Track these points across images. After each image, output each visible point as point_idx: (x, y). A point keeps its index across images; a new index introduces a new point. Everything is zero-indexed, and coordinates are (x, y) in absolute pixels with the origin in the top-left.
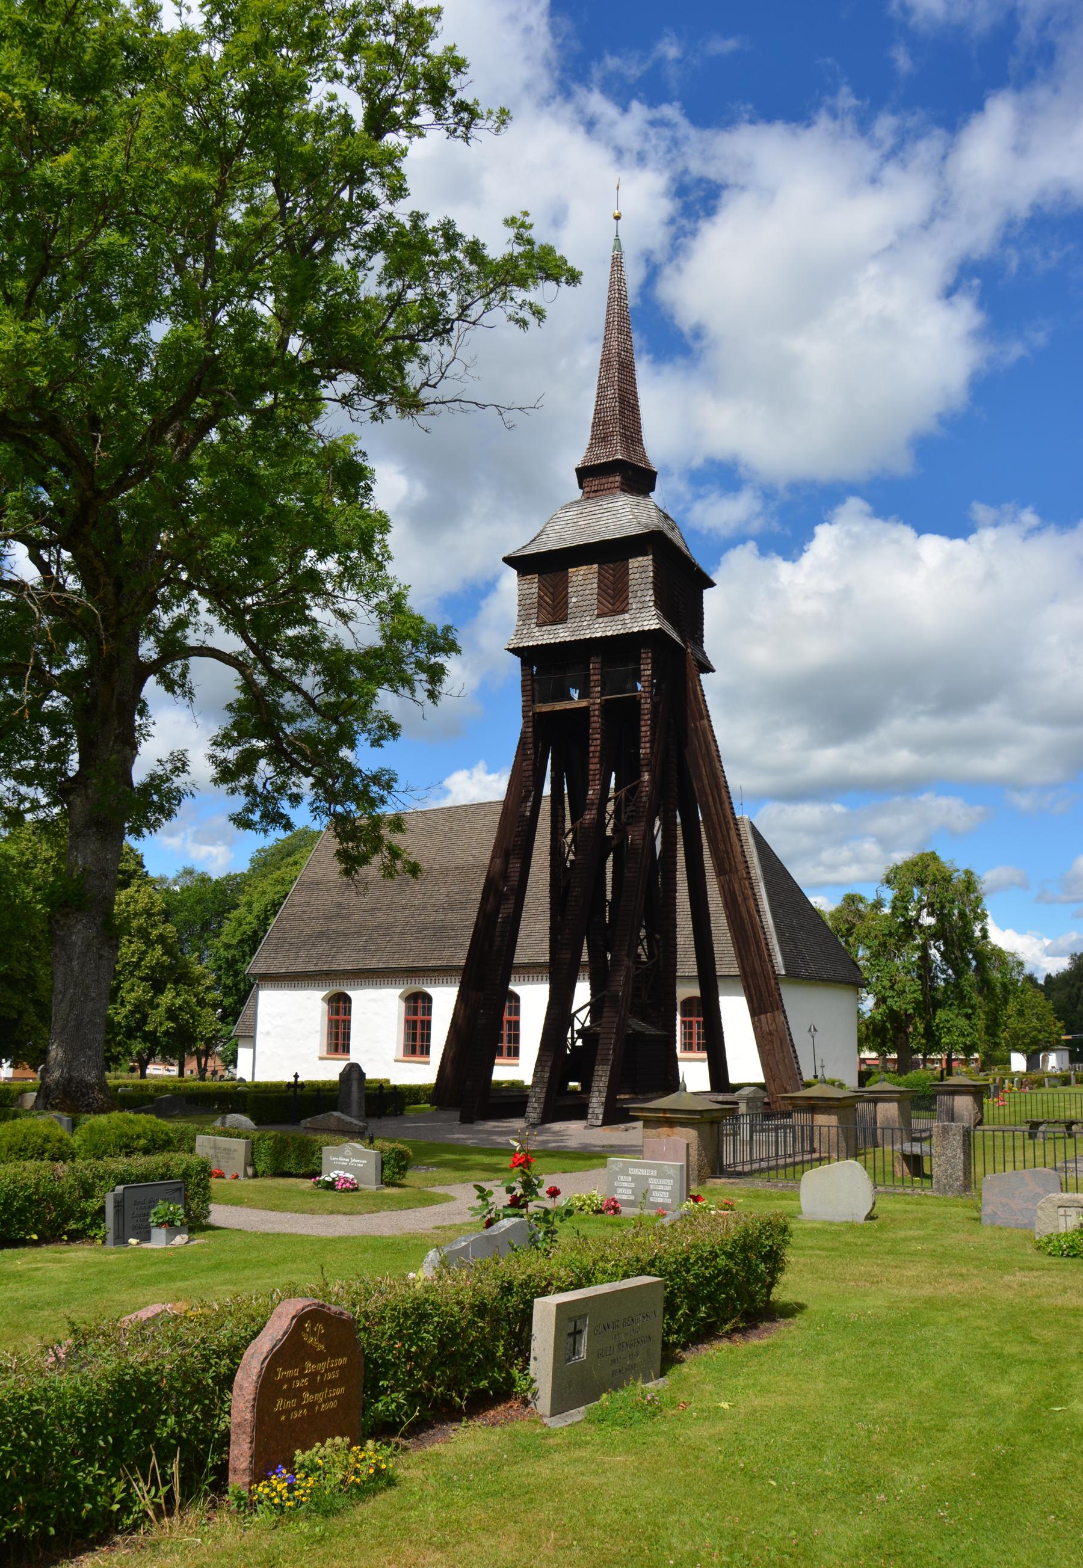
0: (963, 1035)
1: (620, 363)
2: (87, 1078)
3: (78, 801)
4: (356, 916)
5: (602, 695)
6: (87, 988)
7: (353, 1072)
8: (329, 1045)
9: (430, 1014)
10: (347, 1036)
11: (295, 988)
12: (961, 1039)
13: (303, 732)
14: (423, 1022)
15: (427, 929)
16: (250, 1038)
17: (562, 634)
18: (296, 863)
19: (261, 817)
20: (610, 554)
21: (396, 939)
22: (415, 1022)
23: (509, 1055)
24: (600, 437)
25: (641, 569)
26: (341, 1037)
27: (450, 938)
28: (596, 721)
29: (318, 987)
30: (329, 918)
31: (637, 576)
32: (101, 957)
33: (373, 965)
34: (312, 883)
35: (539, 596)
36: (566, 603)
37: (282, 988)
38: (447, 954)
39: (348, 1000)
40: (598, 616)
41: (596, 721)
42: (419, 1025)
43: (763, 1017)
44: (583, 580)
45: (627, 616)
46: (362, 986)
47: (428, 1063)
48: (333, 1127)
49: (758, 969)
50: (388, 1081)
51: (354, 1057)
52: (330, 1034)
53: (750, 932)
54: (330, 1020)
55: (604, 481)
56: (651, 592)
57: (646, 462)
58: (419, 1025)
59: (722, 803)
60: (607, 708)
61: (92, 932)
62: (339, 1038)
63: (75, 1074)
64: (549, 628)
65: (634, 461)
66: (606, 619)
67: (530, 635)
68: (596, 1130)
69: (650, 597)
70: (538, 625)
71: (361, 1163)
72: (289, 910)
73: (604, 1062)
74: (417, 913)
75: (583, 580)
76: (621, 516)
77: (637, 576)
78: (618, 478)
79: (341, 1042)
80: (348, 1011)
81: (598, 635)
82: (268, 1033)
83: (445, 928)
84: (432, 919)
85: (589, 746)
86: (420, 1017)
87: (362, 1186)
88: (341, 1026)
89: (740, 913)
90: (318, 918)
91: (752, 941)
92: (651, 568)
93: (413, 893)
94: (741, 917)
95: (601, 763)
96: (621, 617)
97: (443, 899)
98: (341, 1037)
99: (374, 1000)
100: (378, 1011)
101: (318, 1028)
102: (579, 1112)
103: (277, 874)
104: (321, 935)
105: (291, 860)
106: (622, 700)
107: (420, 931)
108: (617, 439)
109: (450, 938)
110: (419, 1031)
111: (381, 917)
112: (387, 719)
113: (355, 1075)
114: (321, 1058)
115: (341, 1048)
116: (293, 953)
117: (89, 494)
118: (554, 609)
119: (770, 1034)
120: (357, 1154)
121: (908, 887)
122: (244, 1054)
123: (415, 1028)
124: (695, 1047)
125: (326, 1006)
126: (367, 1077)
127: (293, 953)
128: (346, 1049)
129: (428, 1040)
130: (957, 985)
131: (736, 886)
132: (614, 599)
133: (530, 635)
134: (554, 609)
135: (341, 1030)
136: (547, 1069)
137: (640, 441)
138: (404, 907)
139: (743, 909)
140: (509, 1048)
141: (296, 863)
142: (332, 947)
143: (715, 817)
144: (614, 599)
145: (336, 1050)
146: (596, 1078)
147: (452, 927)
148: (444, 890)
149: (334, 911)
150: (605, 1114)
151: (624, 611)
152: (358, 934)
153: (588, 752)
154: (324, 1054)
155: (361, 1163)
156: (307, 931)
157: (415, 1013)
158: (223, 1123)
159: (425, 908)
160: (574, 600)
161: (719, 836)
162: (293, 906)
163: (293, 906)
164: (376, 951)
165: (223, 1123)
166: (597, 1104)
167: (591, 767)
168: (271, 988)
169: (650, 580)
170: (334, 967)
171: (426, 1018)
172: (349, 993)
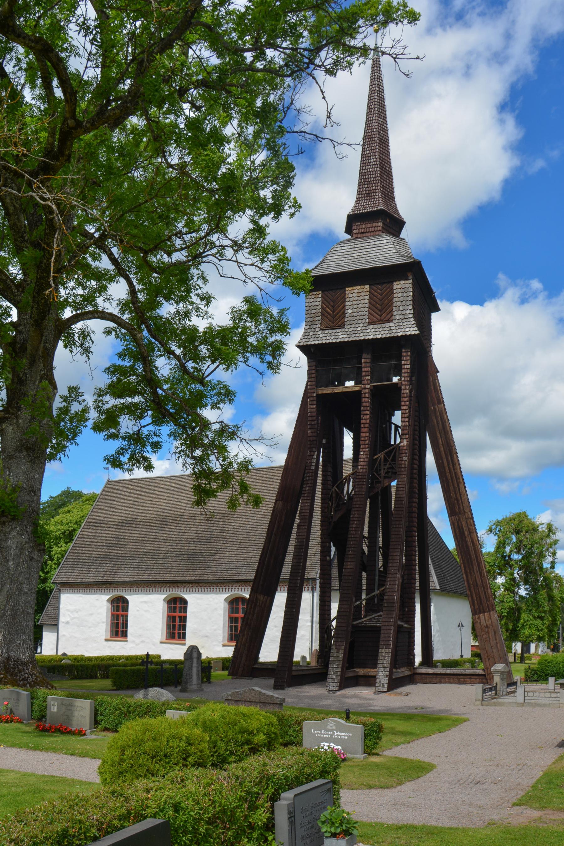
0: (538, 630)
1: (380, 139)
2: (22, 657)
3: (10, 429)
4: (130, 545)
5: (371, 382)
6: (21, 584)
7: (193, 652)
8: (112, 631)
9: (185, 611)
10: (125, 625)
11: (87, 593)
12: (537, 633)
13: (166, 394)
14: (180, 617)
15: (183, 555)
16: (54, 625)
17: (341, 336)
18: (69, 512)
19: (129, 459)
20: (378, 278)
21: (161, 561)
22: (174, 617)
23: (179, 638)
24: (364, 192)
25: (403, 289)
26: (120, 626)
27: (200, 561)
28: (366, 401)
29: (104, 593)
30: (110, 546)
31: (400, 295)
32: (31, 559)
33: (145, 578)
34: (96, 522)
35: (322, 308)
36: (344, 313)
37: (94, 593)
38: (198, 572)
39: (125, 602)
40: (369, 324)
41: (366, 401)
42: (177, 619)
43: (482, 615)
44: (357, 298)
45: (392, 324)
46: (136, 593)
47: (127, 641)
48: (254, 700)
49: (479, 583)
50: (159, 656)
51: (190, 640)
52: (112, 624)
53: (473, 556)
54: (112, 615)
55: (369, 225)
56: (411, 307)
57: (398, 214)
58: (177, 619)
59: (454, 465)
60: (375, 392)
61: (25, 538)
62: (119, 628)
63: (13, 654)
64: (330, 331)
65: (391, 212)
66: (375, 326)
67: (316, 337)
68: (382, 695)
69: (409, 311)
70: (322, 329)
71: (345, 736)
72: (81, 540)
73: (388, 646)
74: (175, 544)
75: (357, 298)
76: (381, 251)
77: (400, 295)
78: (380, 224)
79: (120, 629)
80: (126, 609)
81: (370, 337)
82: (68, 623)
83: (196, 554)
84: (186, 548)
85: (360, 419)
86: (178, 614)
87: (349, 756)
88: (121, 619)
89: (466, 542)
90: (103, 546)
91: (475, 562)
92: (411, 290)
93: (171, 530)
94: (467, 545)
95: (370, 431)
96: (387, 325)
97: (193, 535)
98: (120, 626)
99: (145, 602)
100: (147, 610)
101: (104, 620)
102: (369, 681)
103: (57, 518)
104: (105, 557)
105: (66, 509)
106: (377, 389)
107: (178, 556)
108: (378, 195)
109: (200, 561)
110: (177, 623)
111: (149, 546)
112: (225, 387)
113: (195, 655)
114: (106, 640)
115: (120, 633)
116: (85, 569)
117: (71, 122)
118: (333, 317)
119: (487, 627)
120: (339, 728)
121: (509, 534)
122: (48, 637)
123: (118, 620)
124: (177, 635)
125: (110, 605)
126: (203, 657)
127: (85, 569)
128: (183, 636)
129: (126, 627)
130: (535, 599)
131: (463, 523)
132: (381, 311)
133: (316, 337)
134: (333, 317)
135: (120, 622)
136: (341, 651)
137: (393, 198)
138: (165, 540)
139: (468, 539)
140: (179, 634)
141: (69, 512)
142: (114, 565)
143: (448, 474)
144: (381, 311)
145: (117, 634)
146: (380, 658)
147: (202, 555)
148: (193, 529)
149: (114, 542)
150: (389, 684)
151: (389, 321)
152: (133, 557)
153: (360, 424)
154: (109, 637)
155: (345, 736)
156: (95, 554)
157: (118, 610)
158: (146, 695)
159: (180, 541)
160: (350, 311)
161: (451, 488)
162: (83, 537)
163: (83, 537)
164: (147, 569)
165: (146, 695)
166: (382, 675)
167: (362, 434)
168: (70, 593)
169: (410, 298)
170: (117, 579)
171: (182, 614)
172: (127, 597)
